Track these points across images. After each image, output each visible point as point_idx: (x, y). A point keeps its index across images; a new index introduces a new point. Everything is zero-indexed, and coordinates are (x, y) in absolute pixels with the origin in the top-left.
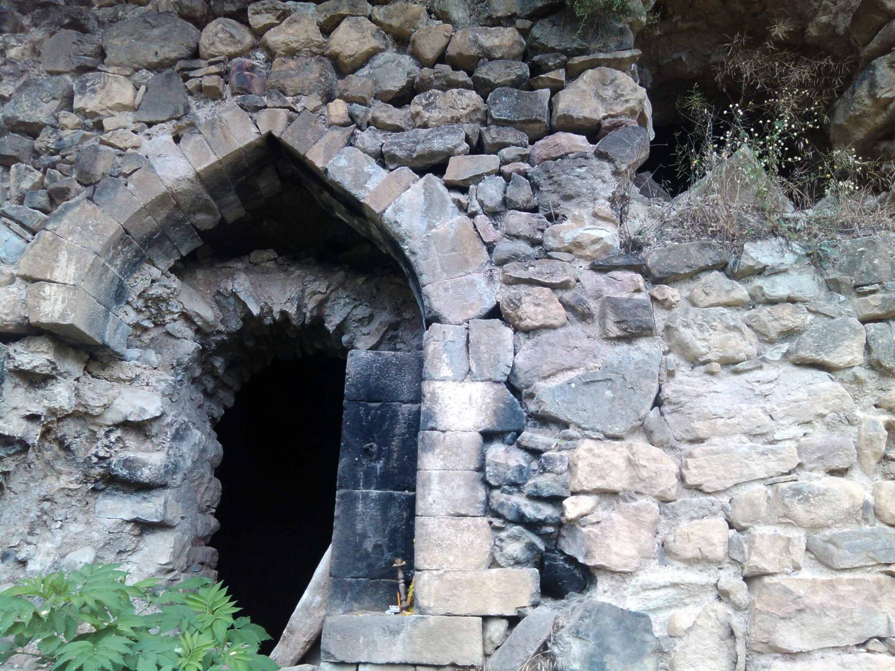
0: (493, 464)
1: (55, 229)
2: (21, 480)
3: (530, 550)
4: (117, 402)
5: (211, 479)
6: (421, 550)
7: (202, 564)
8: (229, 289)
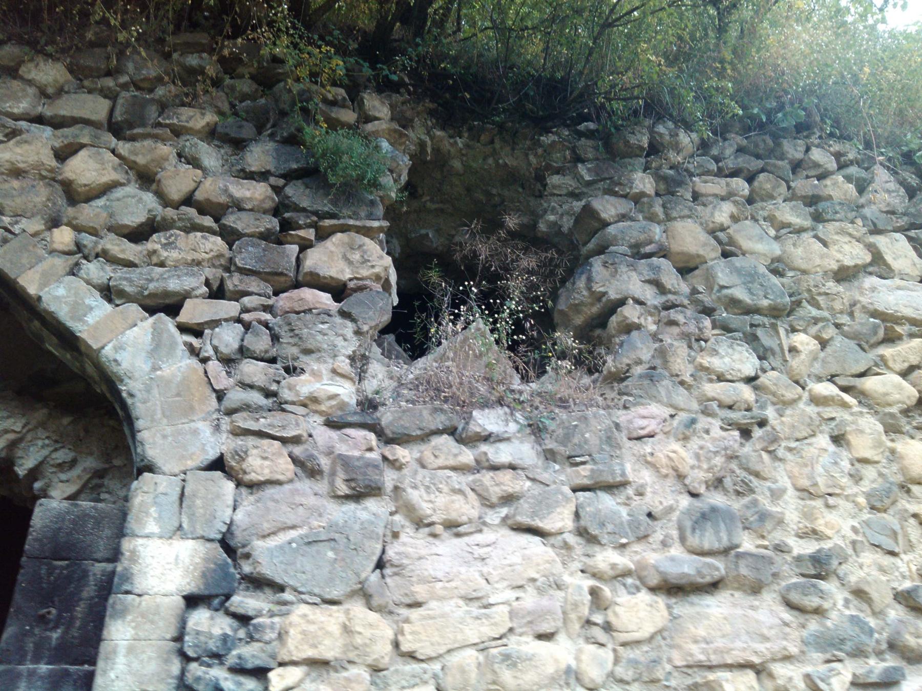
0: (194, 633)
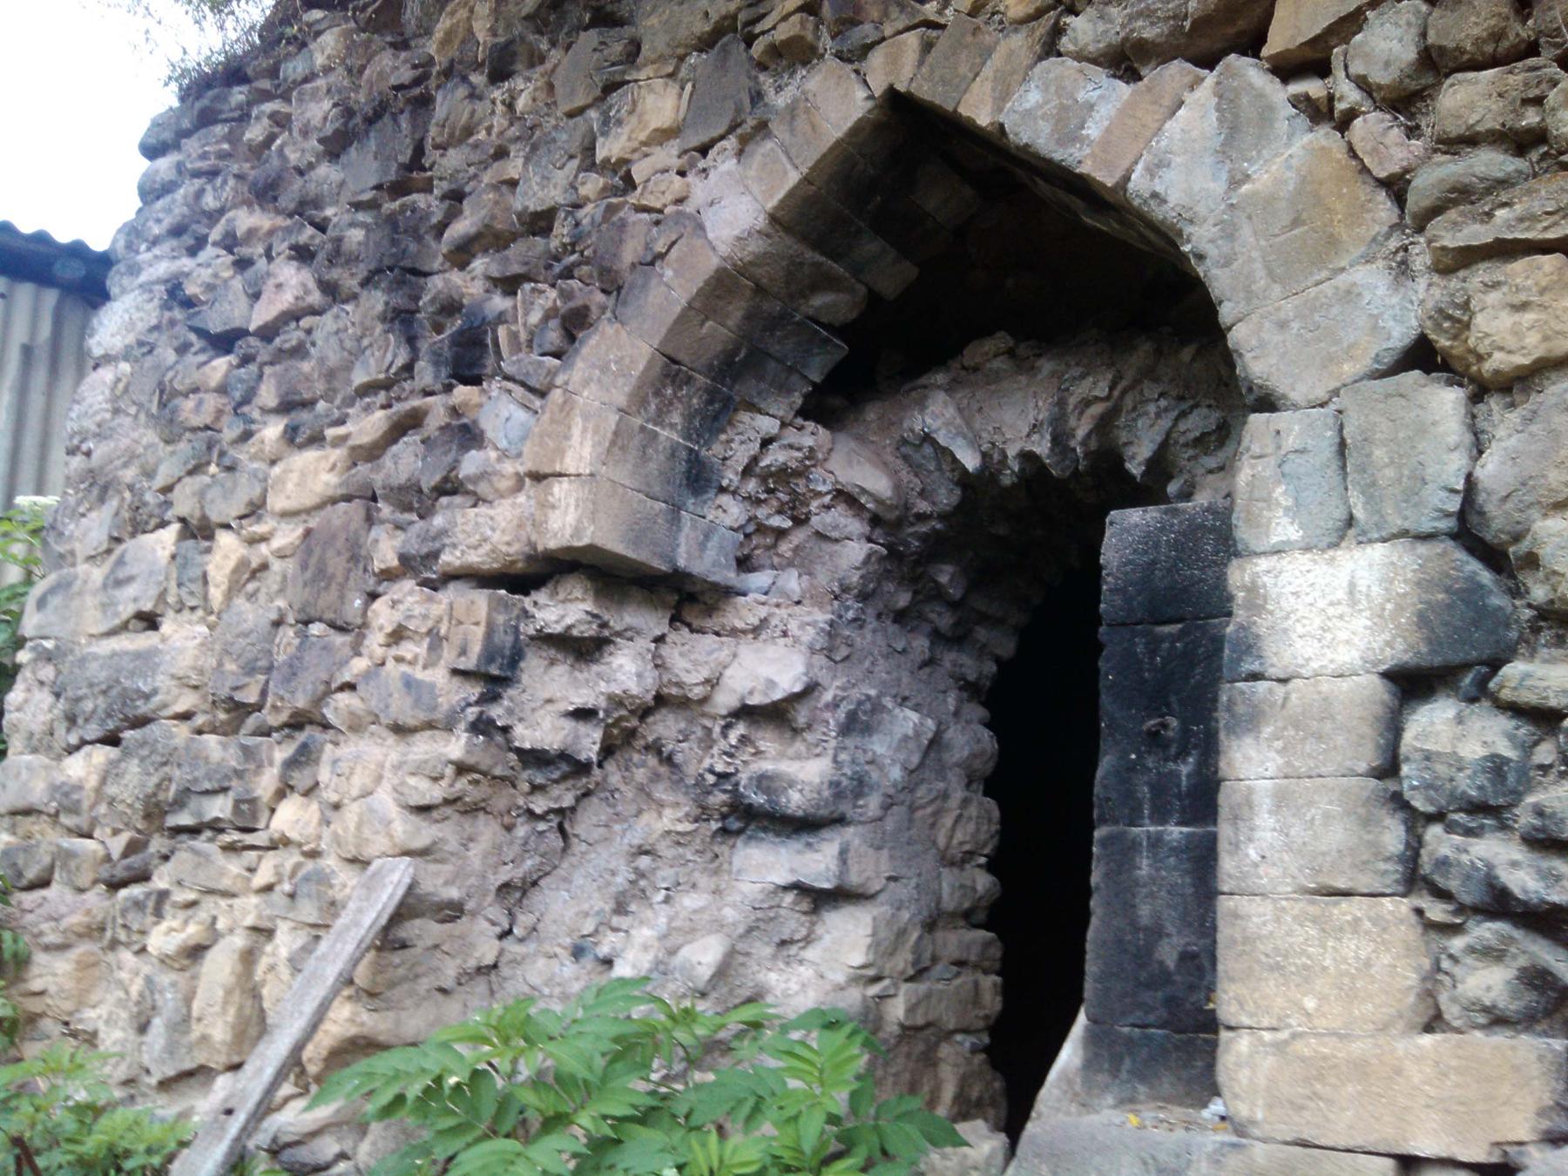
0: (1418, 756)
1: (566, 383)
2: (594, 820)
3: (1535, 988)
4: (728, 673)
5: (965, 802)
6: (1232, 980)
7: (960, 963)
8: (918, 428)
